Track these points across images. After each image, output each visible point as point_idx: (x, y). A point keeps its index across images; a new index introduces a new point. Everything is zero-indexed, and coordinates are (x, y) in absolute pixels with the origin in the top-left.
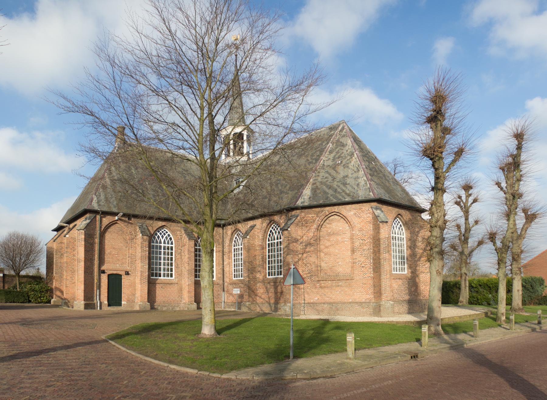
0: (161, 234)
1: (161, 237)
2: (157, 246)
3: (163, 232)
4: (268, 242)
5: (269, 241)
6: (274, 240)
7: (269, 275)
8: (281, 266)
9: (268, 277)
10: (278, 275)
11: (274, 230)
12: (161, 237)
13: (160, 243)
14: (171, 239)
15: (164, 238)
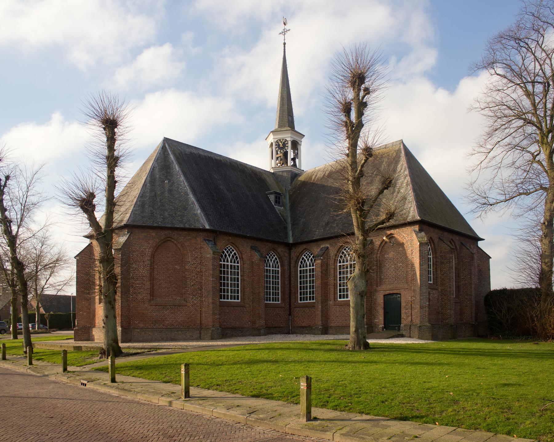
0: (227, 252)
1: (228, 256)
2: (224, 265)
3: (229, 250)
4: (299, 269)
5: (300, 267)
6: (306, 266)
7: (301, 300)
8: (313, 291)
9: (299, 302)
10: (310, 300)
11: (306, 257)
12: (228, 256)
13: (228, 261)
14: (237, 258)
15: (231, 256)
